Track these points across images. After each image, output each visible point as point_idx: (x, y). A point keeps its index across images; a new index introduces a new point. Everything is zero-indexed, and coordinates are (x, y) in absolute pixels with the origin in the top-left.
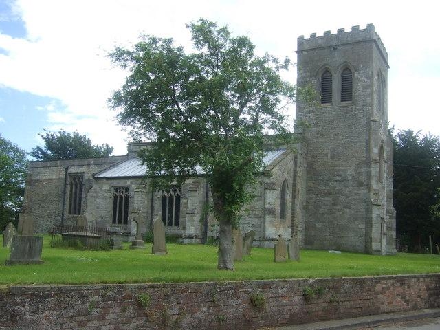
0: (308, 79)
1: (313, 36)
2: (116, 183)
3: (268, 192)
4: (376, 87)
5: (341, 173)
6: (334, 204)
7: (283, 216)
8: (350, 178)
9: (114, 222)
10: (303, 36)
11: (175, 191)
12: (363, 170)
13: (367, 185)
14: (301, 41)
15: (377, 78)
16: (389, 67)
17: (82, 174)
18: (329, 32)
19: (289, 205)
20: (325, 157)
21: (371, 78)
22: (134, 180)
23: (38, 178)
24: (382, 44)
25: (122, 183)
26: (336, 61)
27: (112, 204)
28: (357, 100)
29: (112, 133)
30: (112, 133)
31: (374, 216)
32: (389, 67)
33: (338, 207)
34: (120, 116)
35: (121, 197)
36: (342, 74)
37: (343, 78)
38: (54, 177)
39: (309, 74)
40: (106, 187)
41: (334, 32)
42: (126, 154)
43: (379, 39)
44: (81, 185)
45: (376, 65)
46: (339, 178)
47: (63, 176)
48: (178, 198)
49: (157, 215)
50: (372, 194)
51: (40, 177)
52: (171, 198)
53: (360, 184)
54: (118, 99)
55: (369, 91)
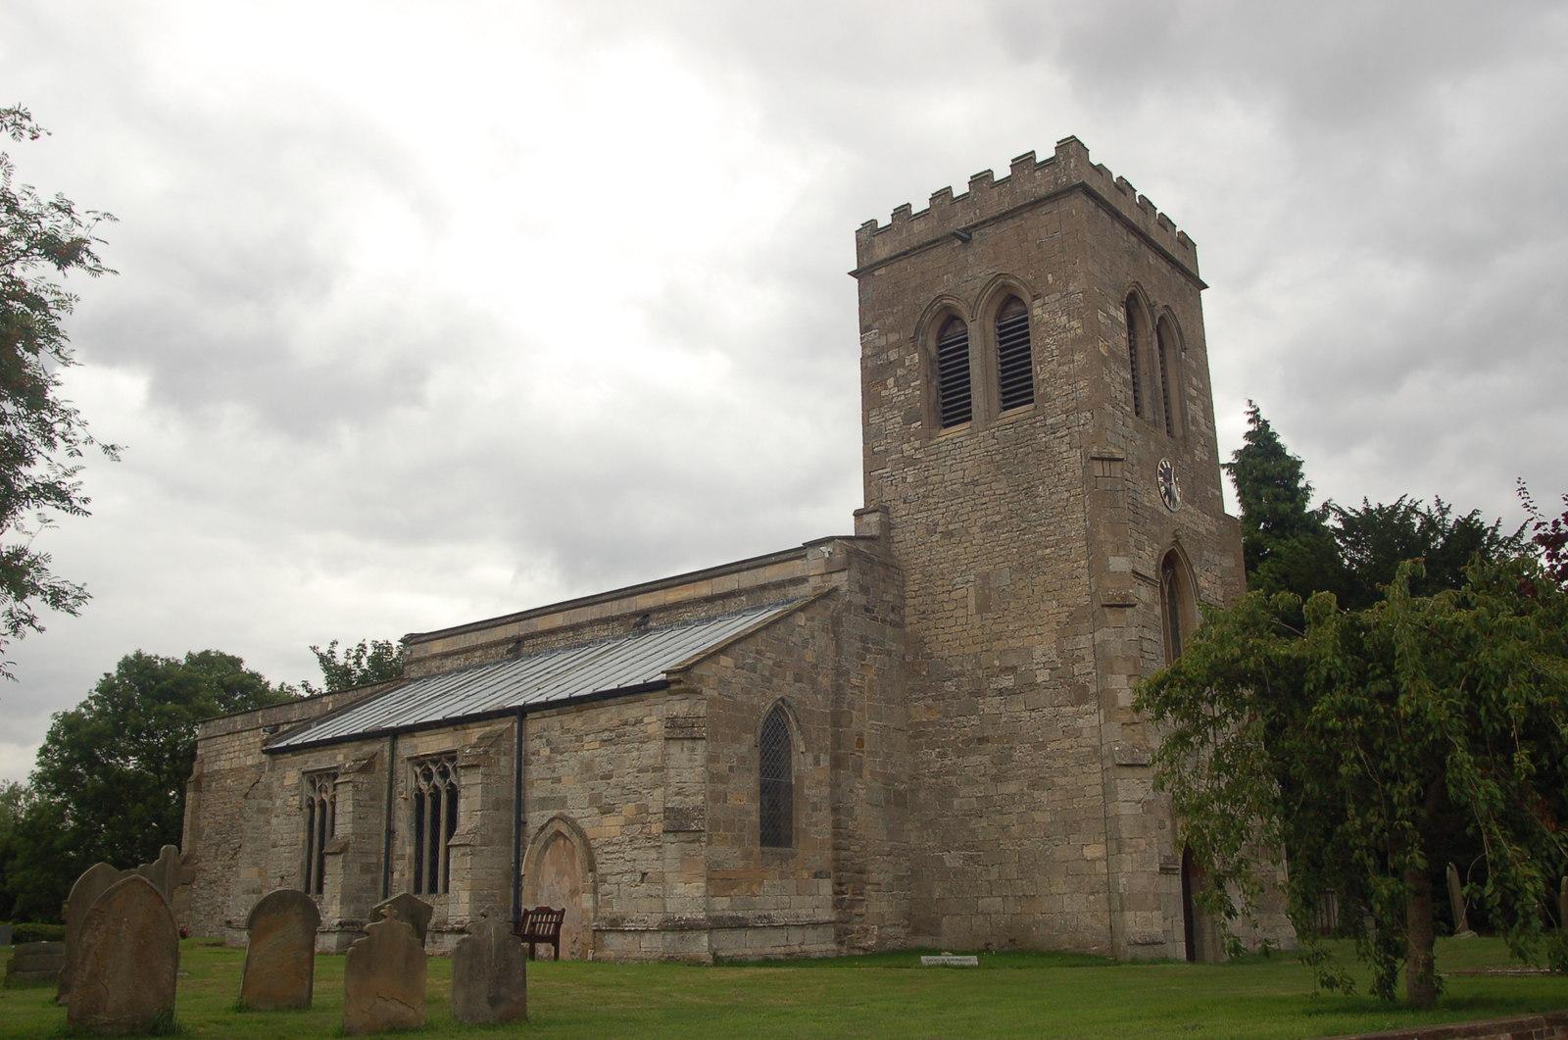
0: (893, 355)
5: (1013, 661)
8: (1042, 676)
11: (445, 774)
12: (1084, 641)
13: (1098, 695)
20: (961, 612)
26: (966, 281)
28: (1046, 398)
33: (1012, 788)
36: (998, 318)
37: (1003, 331)
38: (250, 761)
39: (893, 337)
40: (292, 777)
42: (847, 527)
46: (1008, 681)
49: (402, 857)
51: (223, 764)
53: (1081, 696)
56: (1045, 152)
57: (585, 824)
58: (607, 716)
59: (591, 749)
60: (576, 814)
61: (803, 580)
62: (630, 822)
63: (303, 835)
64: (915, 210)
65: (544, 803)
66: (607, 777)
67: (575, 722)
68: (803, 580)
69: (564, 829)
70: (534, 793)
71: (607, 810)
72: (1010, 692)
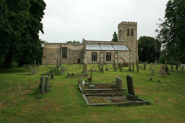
1: (126, 22)
2: (93, 51)
9: (92, 60)
17: (67, 48)
22: (98, 51)
23: (48, 48)
25: (94, 51)
27: (91, 57)
29: (41, 22)
30: (41, 22)
34: (100, 45)
35: (94, 55)
38: (55, 48)
44: (67, 50)
47: (59, 48)
48: (110, 55)
51: (49, 48)
52: (109, 55)
54: (136, 23)
56: (135, 22)
58: (124, 52)
59: (123, 53)
65: (119, 56)
67: (122, 52)
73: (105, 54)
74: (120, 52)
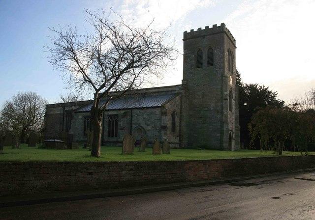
1: (192, 31)
2: (85, 114)
3: (163, 117)
4: (226, 58)
6: (204, 123)
7: (173, 130)
10: (208, 27)
14: (185, 33)
15: (227, 53)
16: (236, 48)
18: (208, 27)
19: (177, 124)
21: (223, 53)
24: (231, 34)
31: (224, 129)
32: (236, 48)
40: (80, 117)
41: (203, 28)
42: (180, 83)
43: (229, 31)
45: (226, 46)
46: (207, 109)
50: (223, 117)
54: (223, 25)
55: (222, 60)
56: (219, 25)
57: (144, 127)
58: (149, 111)
60: (142, 126)
61: (175, 91)
62: (153, 127)
63: (83, 127)
64: (218, 26)
66: (149, 120)
67: (142, 111)
68: (175, 91)
69: (140, 128)
70: (133, 122)
71: (148, 125)
72: (206, 111)
73: (107, 119)
74: (138, 111)
